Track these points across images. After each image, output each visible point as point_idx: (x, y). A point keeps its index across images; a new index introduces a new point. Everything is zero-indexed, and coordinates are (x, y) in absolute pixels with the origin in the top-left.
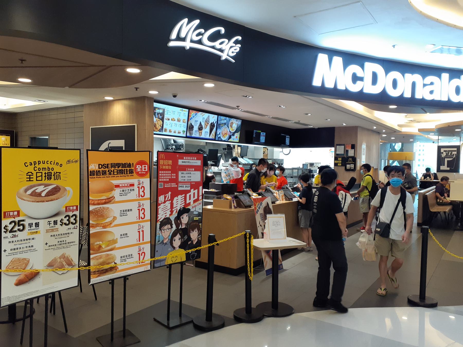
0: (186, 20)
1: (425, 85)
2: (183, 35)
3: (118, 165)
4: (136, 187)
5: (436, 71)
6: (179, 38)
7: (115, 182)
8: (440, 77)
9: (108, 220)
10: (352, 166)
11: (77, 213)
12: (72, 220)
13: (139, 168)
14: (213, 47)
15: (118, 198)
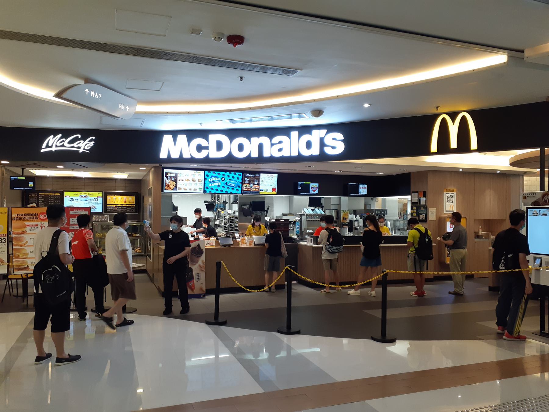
0: (52, 136)
1: (272, 145)
2: (50, 144)
3: (29, 214)
4: (39, 226)
5: (286, 131)
6: (48, 146)
7: (27, 223)
8: (289, 136)
9: (23, 243)
10: (424, 216)
11: (6, 238)
12: (3, 241)
13: (41, 216)
14: (73, 147)
15: (28, 231)
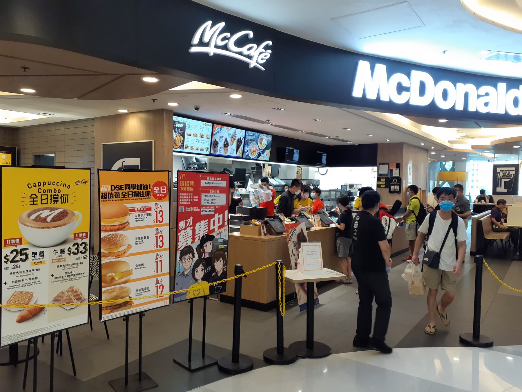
0: (210, 23)
1: (479, 96)
2: (206, 40)
3: (133, 186)
4: (153, 212)
5: (492, 80)
6: (201, 43)
7: (130, 206)
8: (496, 87)
9: (122, 249)
10: (397, 187)
11: (87, 241)
12: (81, 248)
13: (156, 190)
14: (240, 53)
15: (133, 224)
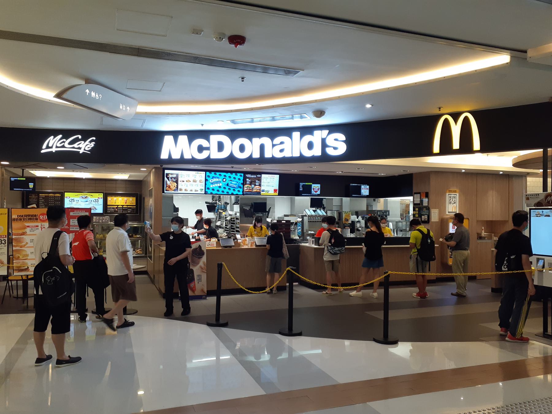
0: (52, 137)
1: (274, 146)
2: (50, 145)
3: (29, 215)
4: (39, 228)
5: (287, 132)
6: (48, 147)
7: (27, 224)
8: (290, 136)
9: (23, 244)
10: (426, 217)
11: (6, 239)
12: (3, 242)
13: (41, 217)
14: (74, 148)
15: (28, 233)
